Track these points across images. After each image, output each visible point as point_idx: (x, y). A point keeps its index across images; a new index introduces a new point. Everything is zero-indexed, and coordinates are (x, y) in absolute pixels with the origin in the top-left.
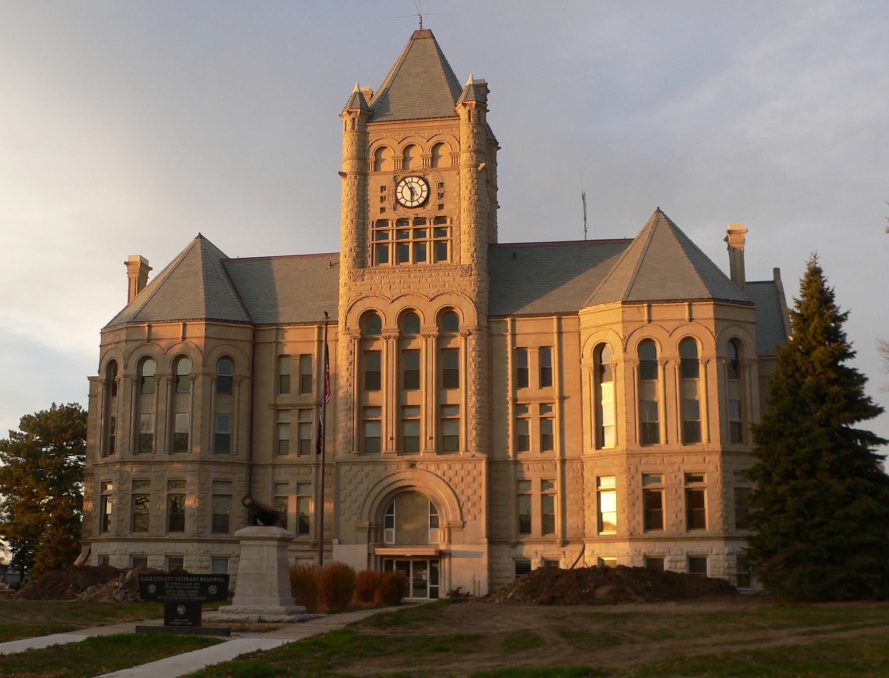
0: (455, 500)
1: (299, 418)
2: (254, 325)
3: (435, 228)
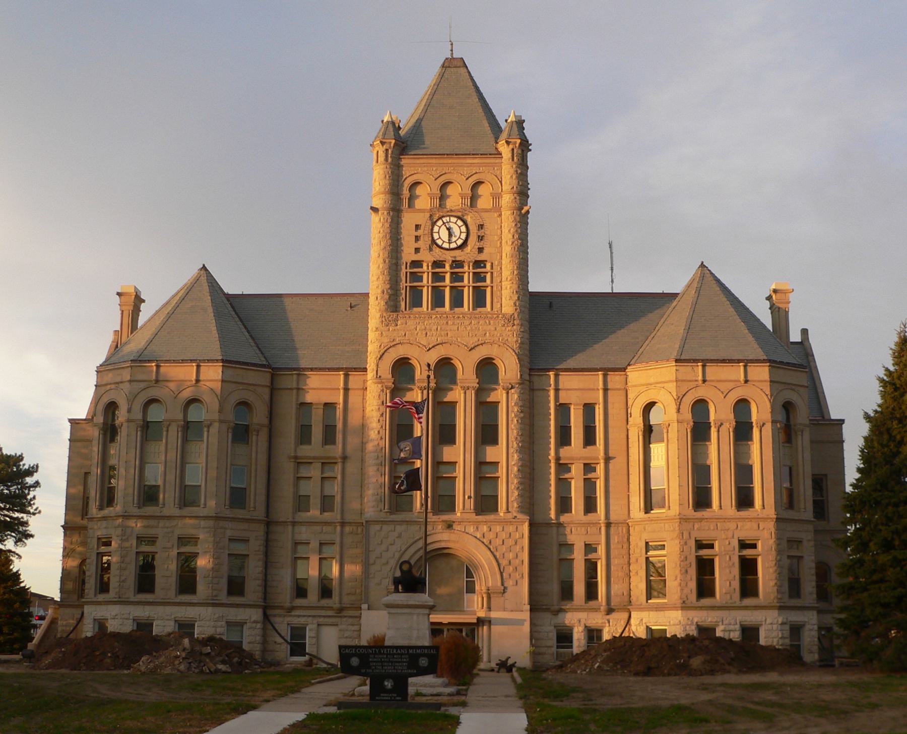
1: (322, 473)
2: (273, 369)
3: (474, 273)
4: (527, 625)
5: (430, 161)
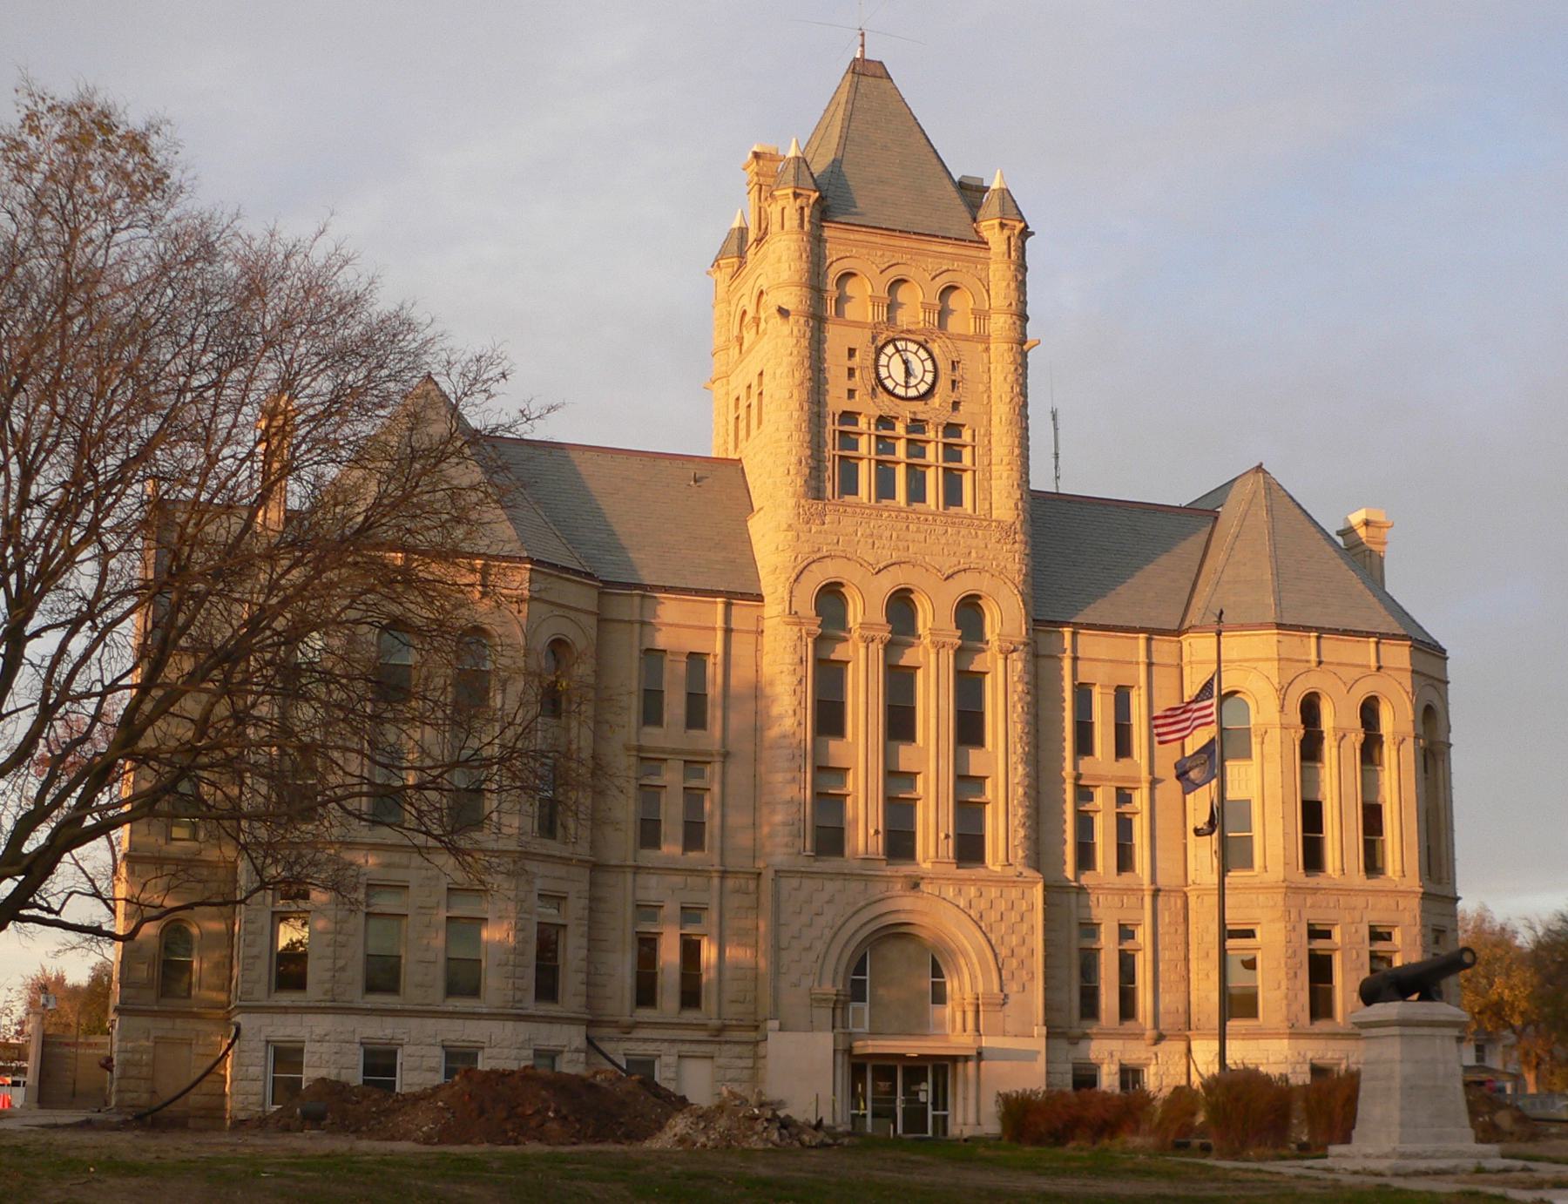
0: (990, 955)
4: (1042, 1059)
5: (873, 239)
